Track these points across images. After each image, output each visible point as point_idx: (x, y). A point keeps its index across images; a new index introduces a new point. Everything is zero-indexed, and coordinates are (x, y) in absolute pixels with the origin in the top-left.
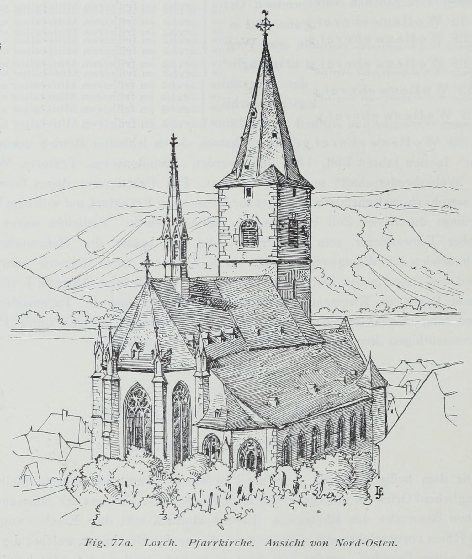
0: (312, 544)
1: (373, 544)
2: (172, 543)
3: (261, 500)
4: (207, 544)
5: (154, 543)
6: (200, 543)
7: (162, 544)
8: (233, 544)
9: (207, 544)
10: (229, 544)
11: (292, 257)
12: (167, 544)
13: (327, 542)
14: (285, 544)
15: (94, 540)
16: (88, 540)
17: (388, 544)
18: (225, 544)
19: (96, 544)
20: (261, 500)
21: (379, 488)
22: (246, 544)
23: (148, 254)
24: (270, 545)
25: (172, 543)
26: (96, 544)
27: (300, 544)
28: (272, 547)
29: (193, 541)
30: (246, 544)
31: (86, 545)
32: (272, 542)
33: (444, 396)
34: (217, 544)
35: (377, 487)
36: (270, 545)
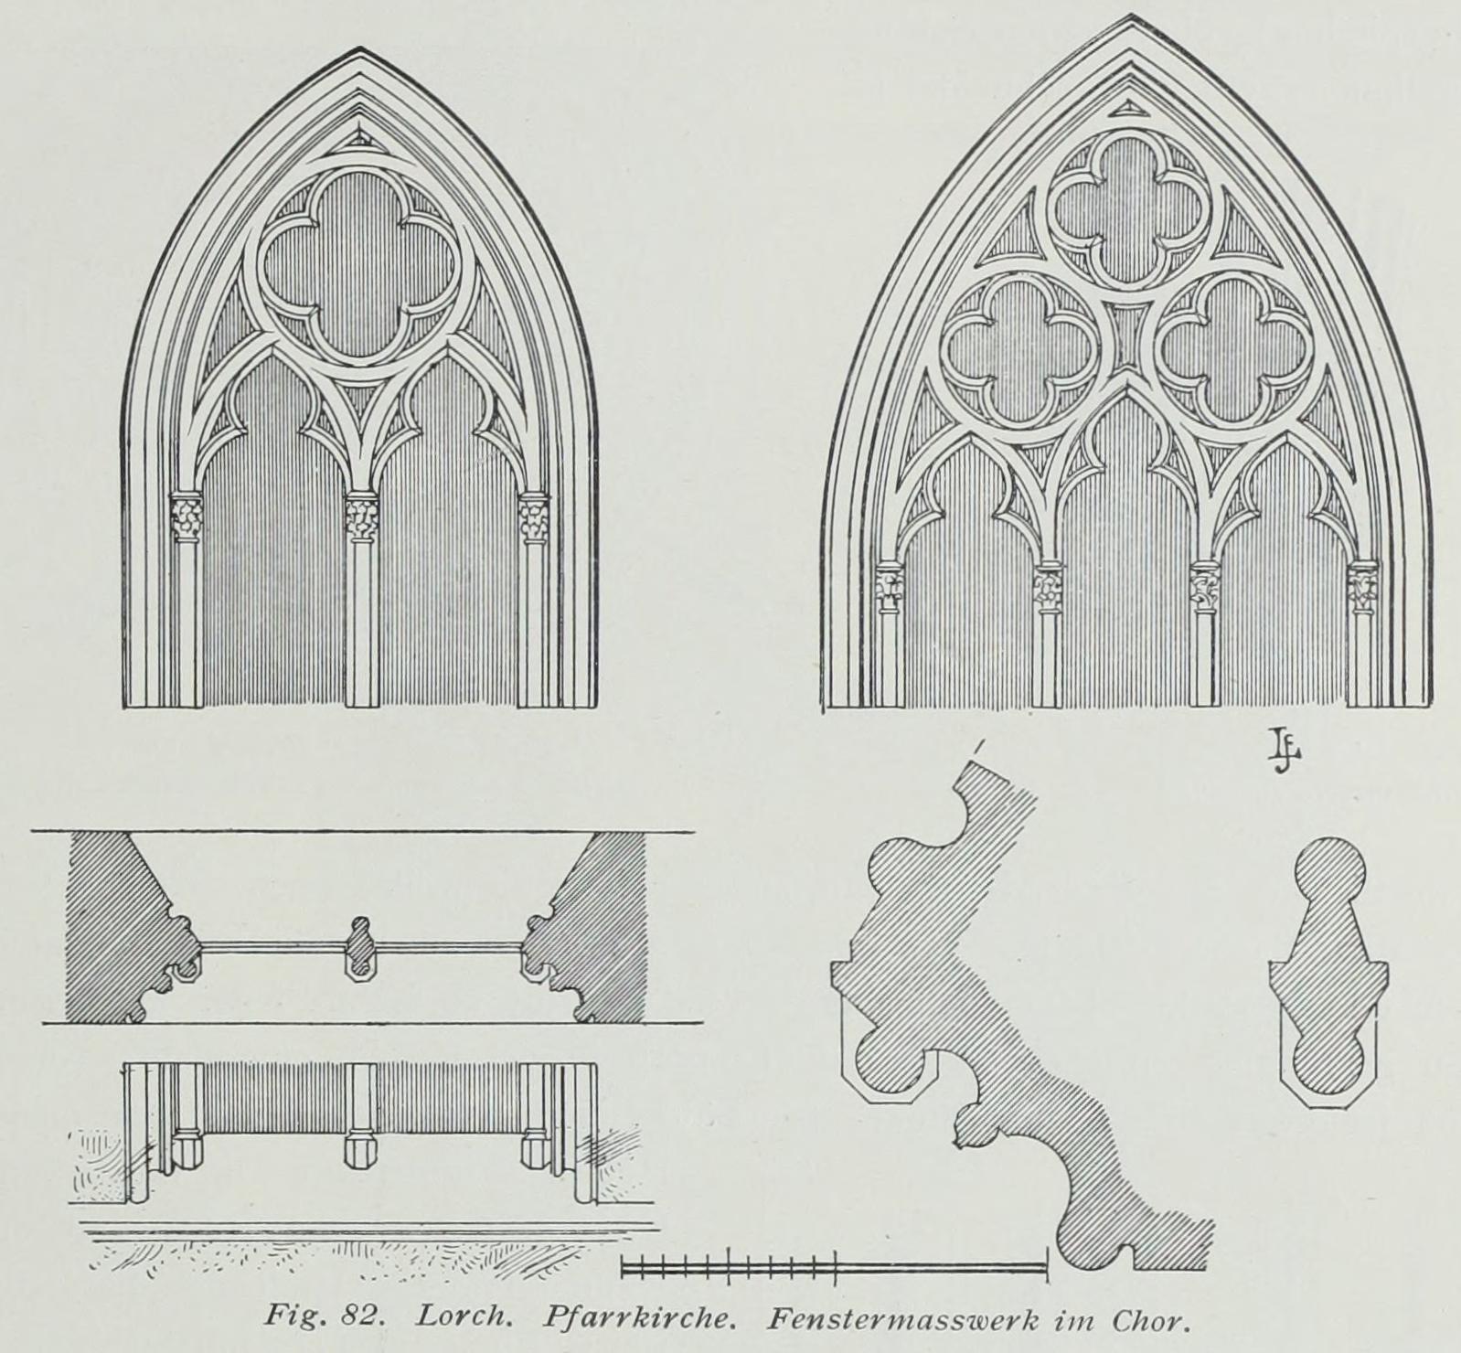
2: (496, 1316)
4: (599, 1319)
5: (447, 1316)
6: (578, 1318)
7: (468, 1319)
9: (599, 1319)
10: (662, 1320)
11: (1069, 1220)
12: (692, 1320)
13: (1092, 1318)
14: (842, 1322)
15: (292, 1308)
16: (275, 1306)
17: (806, 1322)
18: (651, 1320)
19: (299, 1318)
21: (1283, 733)
22: (713, 1320)
23: (1211, 496)
25: (496, 1316)
26: (299, 1318)
29: (560, 1311)
30: (713, 1320)
31: (270, 1322)
32: (706, 1313)
34: (630, 1320)
35: (1277, 730)
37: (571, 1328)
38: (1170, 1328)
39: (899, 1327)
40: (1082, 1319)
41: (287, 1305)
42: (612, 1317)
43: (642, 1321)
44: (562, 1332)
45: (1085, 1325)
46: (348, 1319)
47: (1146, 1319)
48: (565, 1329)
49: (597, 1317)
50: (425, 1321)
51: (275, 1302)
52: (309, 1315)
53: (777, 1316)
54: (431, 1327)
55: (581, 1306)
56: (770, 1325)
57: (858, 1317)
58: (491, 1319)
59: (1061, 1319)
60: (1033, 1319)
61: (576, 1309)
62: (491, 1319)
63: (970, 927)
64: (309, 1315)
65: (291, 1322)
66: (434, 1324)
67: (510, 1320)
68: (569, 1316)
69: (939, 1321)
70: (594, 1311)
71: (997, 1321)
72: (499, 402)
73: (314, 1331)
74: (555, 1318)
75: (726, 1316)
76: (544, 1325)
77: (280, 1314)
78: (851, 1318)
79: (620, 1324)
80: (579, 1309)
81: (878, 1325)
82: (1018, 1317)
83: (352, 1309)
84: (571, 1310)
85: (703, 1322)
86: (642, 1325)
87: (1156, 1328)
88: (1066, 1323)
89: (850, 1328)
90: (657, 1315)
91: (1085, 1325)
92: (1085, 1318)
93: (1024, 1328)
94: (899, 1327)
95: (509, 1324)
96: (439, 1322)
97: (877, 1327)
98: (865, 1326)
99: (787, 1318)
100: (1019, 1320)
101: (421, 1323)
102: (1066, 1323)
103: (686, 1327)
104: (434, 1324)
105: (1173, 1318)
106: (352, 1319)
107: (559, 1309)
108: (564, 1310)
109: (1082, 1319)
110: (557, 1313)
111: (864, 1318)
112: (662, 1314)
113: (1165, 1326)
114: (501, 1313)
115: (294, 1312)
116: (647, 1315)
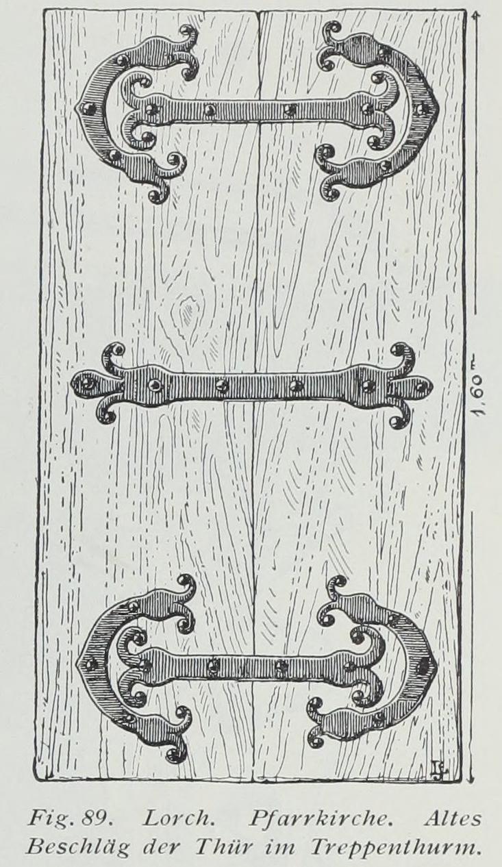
0: (107, 564)
1: (67, 848)
3: (157, 695)
4: (290, 821)
6: (275, 819)
7: (181, 821)
8: (348, 821)
9: (290, 821)
10: (337, 820)
13: (293, 845)
16: (36, 811)
18: (330, 819)
19: (54, 820)
20: (157, 695)
24: (436, 824)
27: (93, 849)
28: (440, 827)
29: (261, 814)
32: (370, 815)
33: (85, 816)
34: (313, 821)
36: (436, 824)
37: (270, 826)
38: (175, 823)
39: (464, 853)
40: (466, 845)
41: (45, 810)
42: (301, 818)
43: (323, 822)
44: (263, 830)
45: (468, 851)
46: (87, 821)
47: (373, 817)
48: (265, 827)
49: (289, 818)
50: (149, 823)
51: (36, 808)
52: (61, 818)
53: (34, 816)
54: (155, 826)
55: (277, 811)
56: (29, 822)
57: (461, 817)
58: (199, 820)
59: (270, 845)
60: (324, 817)
61: (273, 813)
62: (199, 820)
63: (53, 77)
64: (61, 818)
65: (48, 823)
66: (156, 824)
67: (213, 821)
68: (268, 817)
69: (65, 850)
70: (287, 814)
71: (163, 847)
72: (103, 397)
73: (66, 829)
74: (257, 819)
75: (386, 816)
76: (250, 825)
77: (40, 817)
78: (456, 817)
79: (306, 824)
80: (275, 813)
81: (309, 822)
82: (313, 816)
83: (90, 814)
84: (270, 813)
85: (202, 821)
86: (323, 824)
87: (167, 817)
88: (273, 849)
89: (335, 825)
90: (334, 817)
91: (468, 851)
92: (395, 845)
93: (318, 823)
94: (464, 853)
95: (213, 824)
96: (160, 823)
97: (296, 824)
98: (384, 823)
99: (42, 818)
100: (313, 818)
101: (147, 824)
102: (273, 849)
103: (380, 825)
104: (156, 824)
105: (246, 845)
106: (89, 822)
107: (260, 812)
108: (264, 813)
109: (466, 845)
110: (259, 815)
111: (383, 817)
112: (242, 844)
113: (377, 819)
114: (207, 816)
115: (50, 816)
116: (327, 816)
